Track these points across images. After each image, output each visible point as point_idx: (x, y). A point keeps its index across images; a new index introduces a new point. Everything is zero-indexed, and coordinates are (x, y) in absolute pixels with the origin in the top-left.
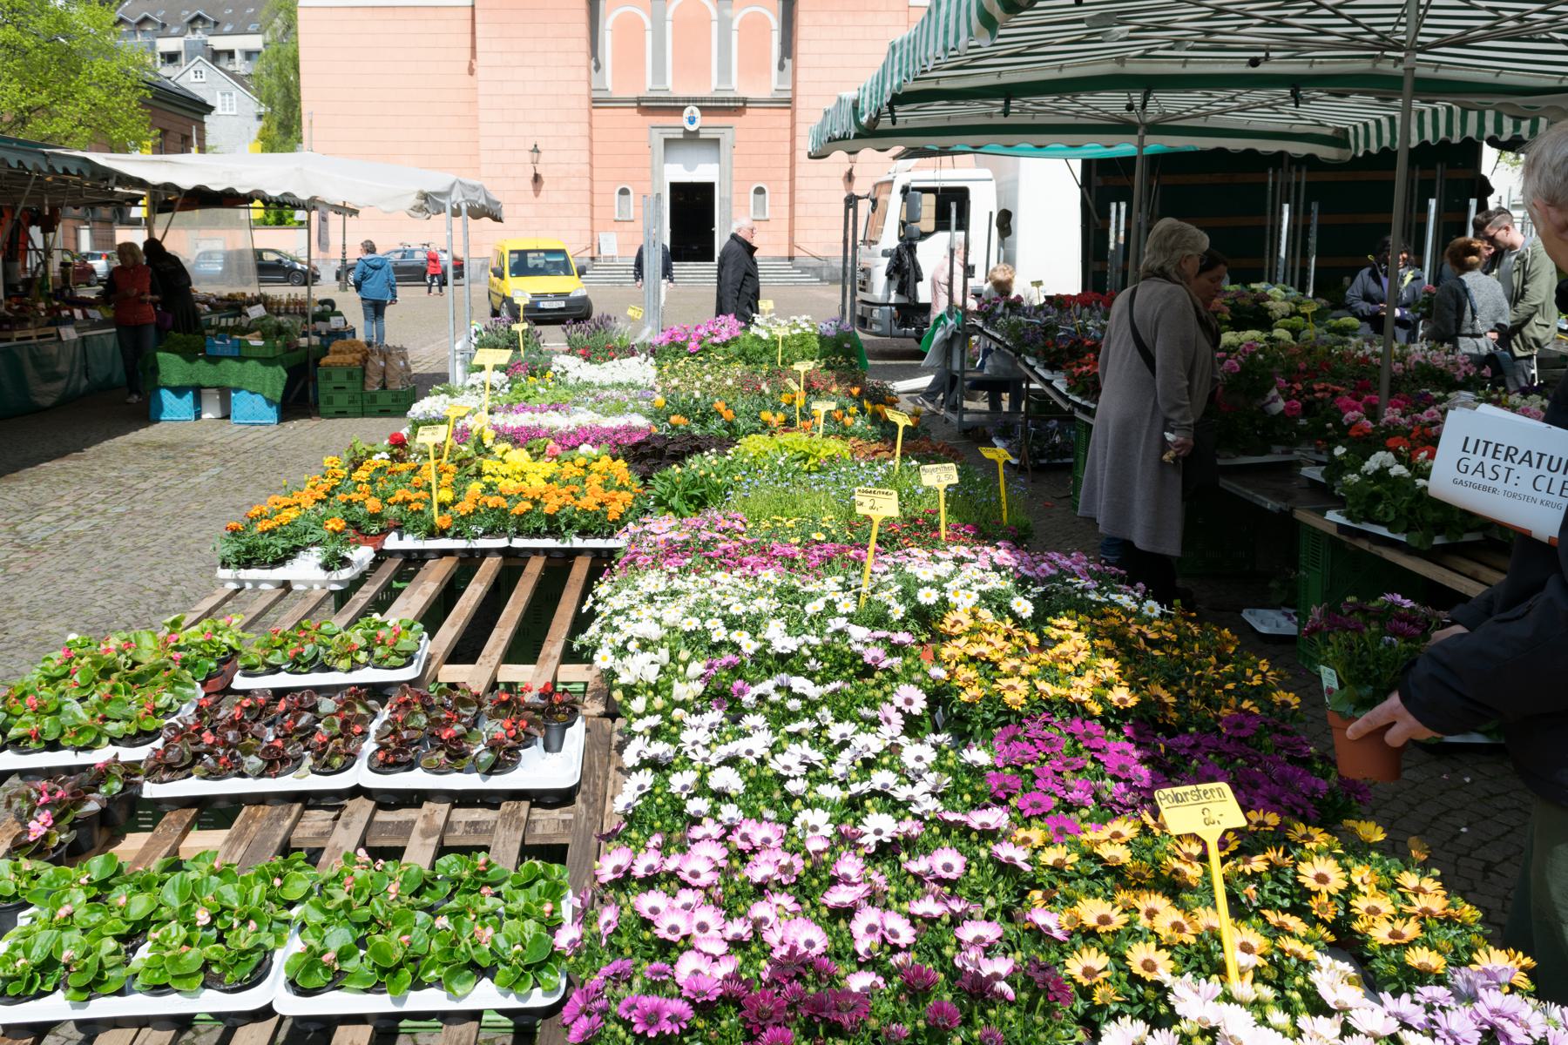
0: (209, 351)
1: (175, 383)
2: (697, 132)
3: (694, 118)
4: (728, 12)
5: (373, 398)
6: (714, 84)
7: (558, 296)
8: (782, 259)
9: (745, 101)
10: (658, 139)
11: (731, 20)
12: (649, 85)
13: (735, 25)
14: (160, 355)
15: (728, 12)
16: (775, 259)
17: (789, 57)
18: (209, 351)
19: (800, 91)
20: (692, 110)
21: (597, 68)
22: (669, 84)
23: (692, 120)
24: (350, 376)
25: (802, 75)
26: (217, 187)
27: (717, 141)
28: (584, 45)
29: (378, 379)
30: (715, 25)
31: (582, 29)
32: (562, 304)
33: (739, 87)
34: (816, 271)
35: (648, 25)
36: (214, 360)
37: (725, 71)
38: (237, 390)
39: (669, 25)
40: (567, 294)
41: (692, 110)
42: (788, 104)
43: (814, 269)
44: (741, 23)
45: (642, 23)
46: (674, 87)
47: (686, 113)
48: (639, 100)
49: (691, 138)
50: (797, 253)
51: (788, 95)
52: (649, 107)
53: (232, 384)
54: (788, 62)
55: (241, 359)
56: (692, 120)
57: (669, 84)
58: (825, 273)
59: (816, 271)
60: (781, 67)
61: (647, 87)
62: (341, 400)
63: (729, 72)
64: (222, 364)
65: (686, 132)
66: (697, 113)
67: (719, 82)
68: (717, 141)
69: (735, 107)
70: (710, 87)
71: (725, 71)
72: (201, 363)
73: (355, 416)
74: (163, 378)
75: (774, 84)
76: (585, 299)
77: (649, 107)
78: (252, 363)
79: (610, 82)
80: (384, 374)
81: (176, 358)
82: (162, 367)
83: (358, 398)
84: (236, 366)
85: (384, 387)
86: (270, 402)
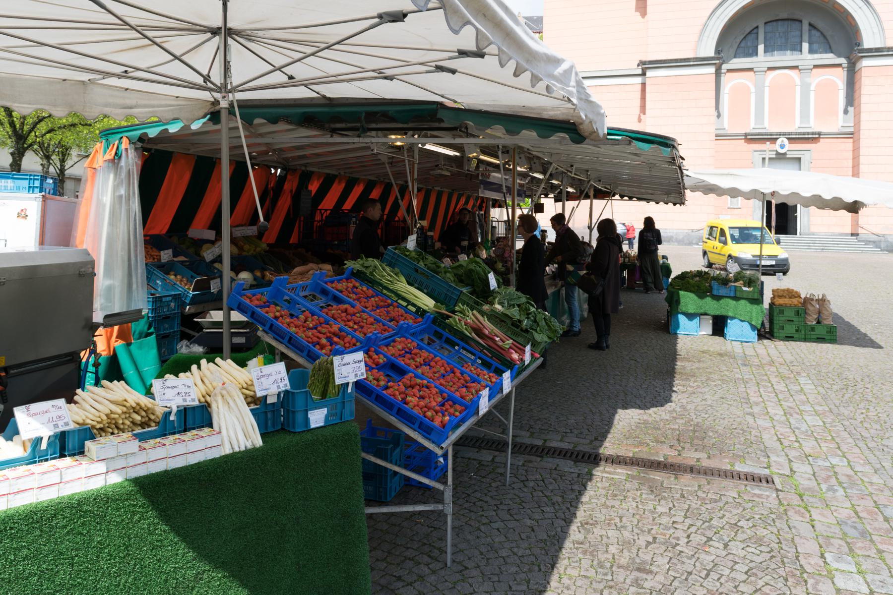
0: (715, 292)
1: (691, 311)
2: (785, 154)
3: (783, 145)
4: (808, 80)
5: (813, 329)
6: (798, 124)
7: (771, 257)
8: (847, 235)
9: (820, 134)
10: (758, 158)
11: (810, 85)
12: (798, 123)
13: (813, 87)
14: (681, 293)
15: (808, 80)
16: (841, 234)
17: (852, 106)
18: (715, 292)
19: (864, 125)
20: (783, 140)
21: (719, 116)
22: (766, 124)
23: (782, 146)
24: (797, 313)
25: (864, 117)
26: (827, 196)
27: (799, 159)
28: (713, 102)
29: (816, 317)
30: (798, 89)
31: (713, 93)
32: (773, 263)
33: (814, 125)
34: (876, 244)
35: (753, 89)
36: (718, 298)
37: (805, 115)
38: (732, 318)
39: (767, 90)
40: (776, 256)
41: (783, 140)
42: (853, 135)
43: (874, 242)
44: (817, 86)
45: (749, 89)
46: (770, 127)
47: (779, 142)
48: (746, 135)
49: (780, 157)
50: (860, 231)
51: (852, 130)
52: (751, 139)
53: (730, 314)
54: (851, 109)
55: (736, 298)
56: (782, 146)
57: (766, 124)
58: (883, 245)
59: (876, 244)
60: (846, 112)
61: (751, 127)
62: (790, 329)
63: (808, 116)
64: (723, 301)
65: (778, 153)
66: (786, 141)
67: (801, 122)
68: (799, 159)
69: (813, 138)
70: (795, 126)
71: (805, 115)
72: (708, 299)
73: (800, 340)
74: (682, 307)
75: (841, 123)
76: (786, 260)
77: (751, 139)
78: (743, 302)
79: (728, 125)
80: (819, 313)
81: (692, 296)
82: (682, 300)
83: (802, 328)
84: (733, 303)
85: (819, 322)
86: (753, 327)
